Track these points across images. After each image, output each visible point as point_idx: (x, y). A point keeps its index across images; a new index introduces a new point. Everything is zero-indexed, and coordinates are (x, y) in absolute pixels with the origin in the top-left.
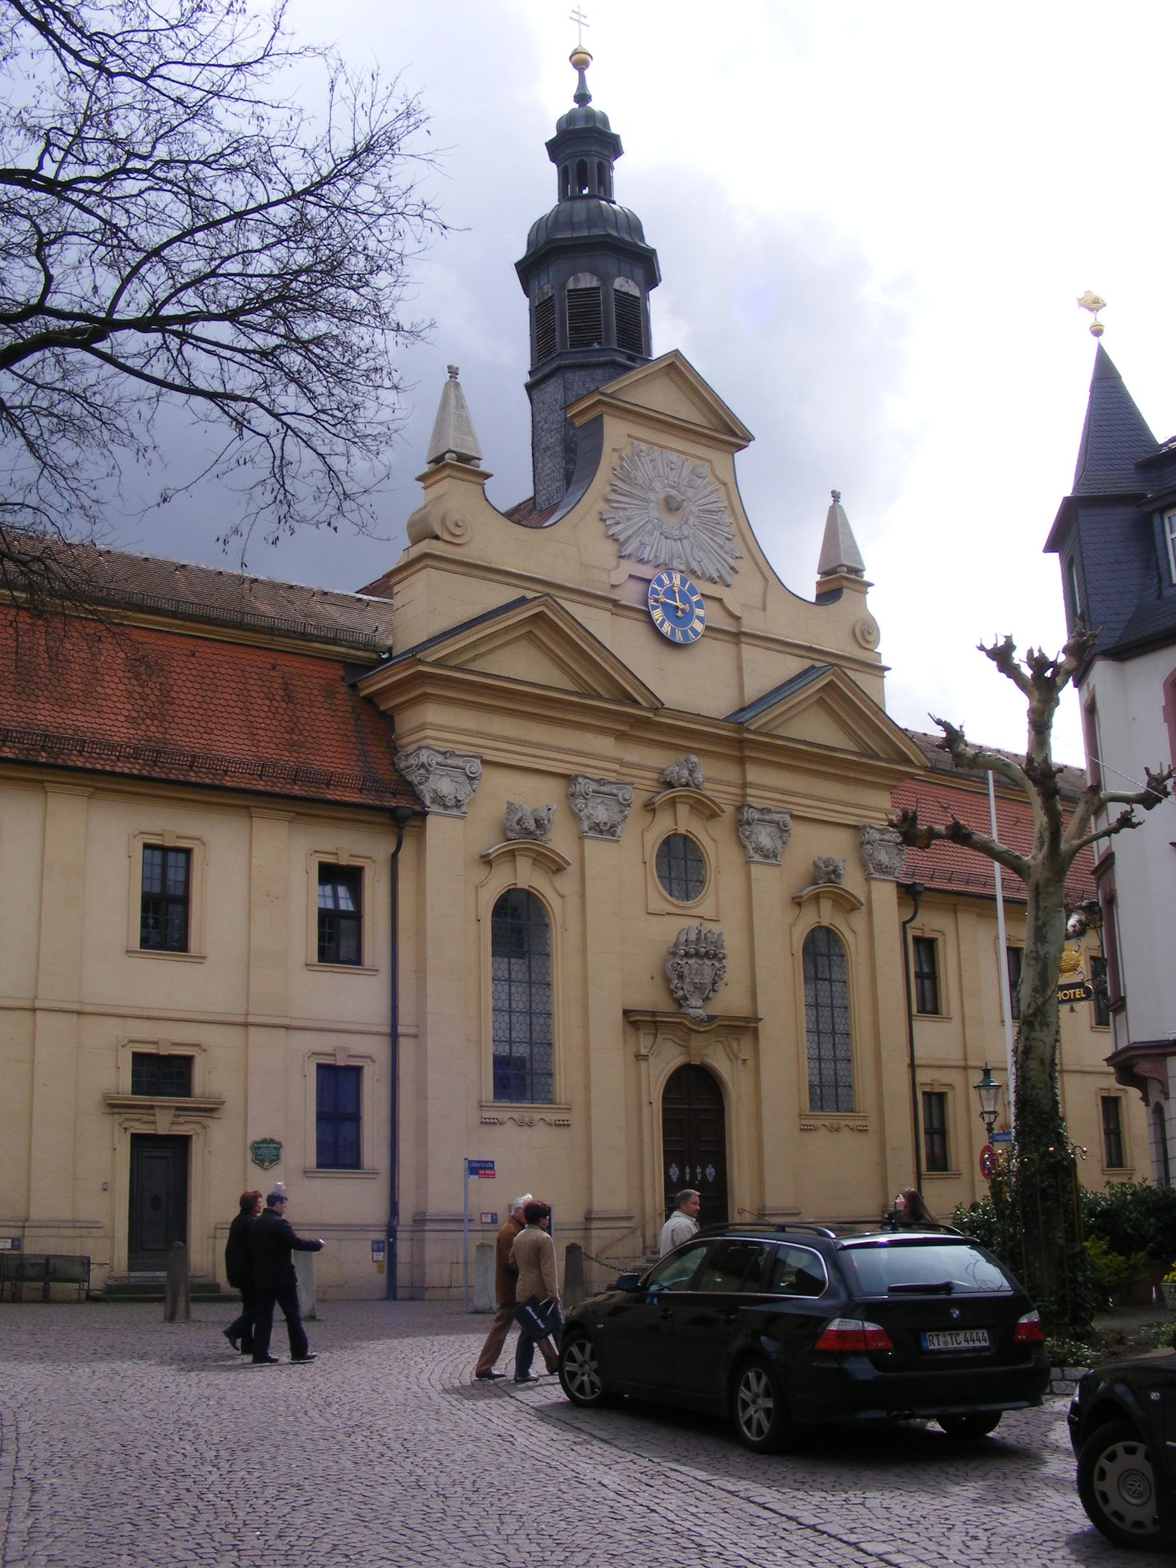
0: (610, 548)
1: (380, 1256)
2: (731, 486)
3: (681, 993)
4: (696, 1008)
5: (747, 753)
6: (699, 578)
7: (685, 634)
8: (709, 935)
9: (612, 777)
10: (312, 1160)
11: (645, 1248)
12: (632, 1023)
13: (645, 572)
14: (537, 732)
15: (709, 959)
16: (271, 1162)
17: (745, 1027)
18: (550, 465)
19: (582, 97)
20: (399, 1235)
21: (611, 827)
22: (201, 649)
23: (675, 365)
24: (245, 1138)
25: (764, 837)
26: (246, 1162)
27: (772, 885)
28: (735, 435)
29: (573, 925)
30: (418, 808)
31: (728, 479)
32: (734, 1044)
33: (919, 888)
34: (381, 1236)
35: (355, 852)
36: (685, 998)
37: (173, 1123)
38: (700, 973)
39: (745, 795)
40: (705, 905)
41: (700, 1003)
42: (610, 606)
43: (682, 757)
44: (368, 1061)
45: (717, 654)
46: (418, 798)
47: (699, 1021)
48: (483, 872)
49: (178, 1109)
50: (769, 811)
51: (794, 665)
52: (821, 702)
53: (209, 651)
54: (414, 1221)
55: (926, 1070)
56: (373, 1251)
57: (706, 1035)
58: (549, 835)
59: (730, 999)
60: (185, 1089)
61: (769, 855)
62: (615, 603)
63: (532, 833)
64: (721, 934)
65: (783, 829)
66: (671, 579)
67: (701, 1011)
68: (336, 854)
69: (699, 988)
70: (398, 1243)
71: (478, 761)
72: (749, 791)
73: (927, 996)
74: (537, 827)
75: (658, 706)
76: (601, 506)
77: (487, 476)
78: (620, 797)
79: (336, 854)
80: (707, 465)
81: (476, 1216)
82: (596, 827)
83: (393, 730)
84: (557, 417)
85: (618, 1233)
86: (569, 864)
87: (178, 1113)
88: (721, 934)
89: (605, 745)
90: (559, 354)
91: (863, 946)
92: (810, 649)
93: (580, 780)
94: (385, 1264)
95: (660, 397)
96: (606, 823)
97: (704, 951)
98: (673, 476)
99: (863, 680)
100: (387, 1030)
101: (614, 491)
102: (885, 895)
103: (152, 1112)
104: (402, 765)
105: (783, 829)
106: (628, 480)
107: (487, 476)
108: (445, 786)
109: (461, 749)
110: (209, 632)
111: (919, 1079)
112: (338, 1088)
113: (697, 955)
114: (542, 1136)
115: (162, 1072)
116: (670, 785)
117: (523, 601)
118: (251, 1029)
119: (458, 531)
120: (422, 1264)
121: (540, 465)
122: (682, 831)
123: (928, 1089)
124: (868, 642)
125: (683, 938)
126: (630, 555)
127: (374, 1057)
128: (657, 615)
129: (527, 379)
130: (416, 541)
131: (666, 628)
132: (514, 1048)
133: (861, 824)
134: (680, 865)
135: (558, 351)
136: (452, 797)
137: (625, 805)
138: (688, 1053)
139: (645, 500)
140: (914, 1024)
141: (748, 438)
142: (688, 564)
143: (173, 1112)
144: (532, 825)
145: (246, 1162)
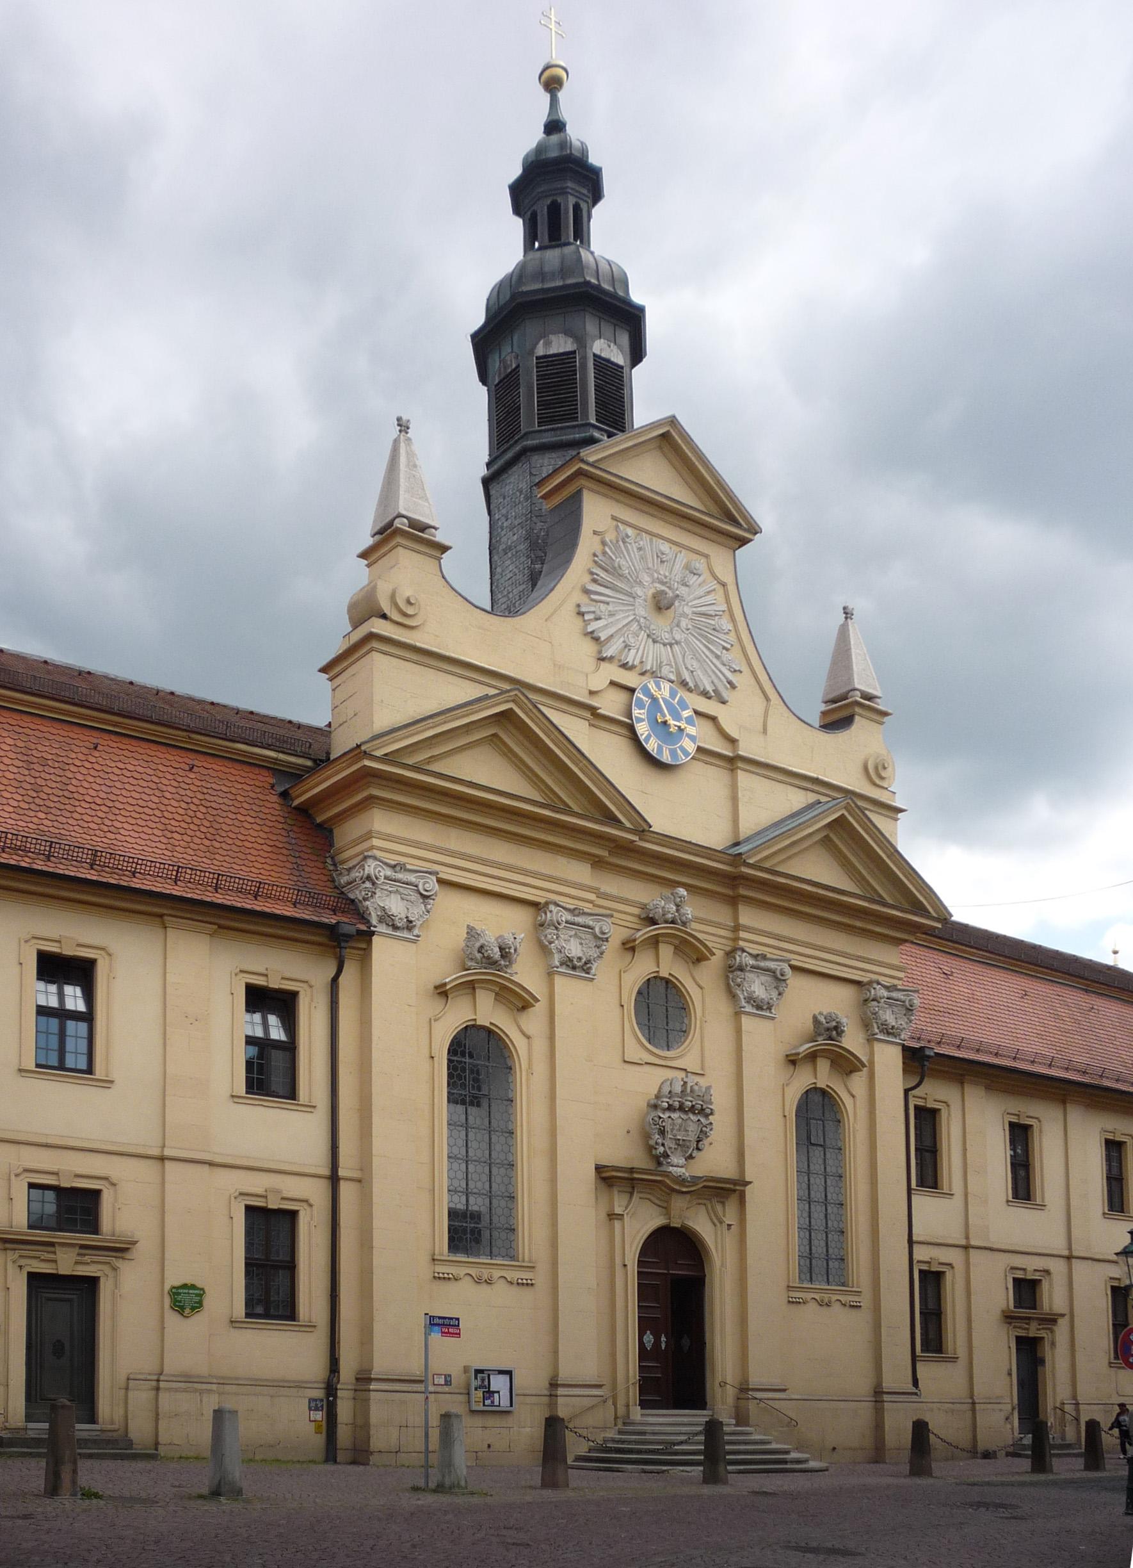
0: (588, 648)
1: (319, 1416)
2: (732, 588)
3: (661, 1149)
4: (678, 1166)
5: (742, 891)
6: (690, 690)
7: (673, 753)
8: (696, 1088)
9: (587, 907)
10: (240, 1309)
11: (616, 1418)
12: (604, 1179)
15: (694, 1113)
16: (193, 1309)
18: (511, 568)
19: (554, 126)
20: (339, 1393)
21: (586, 963)
23: (670, 441)
24: (163, 1282)
25: (758, 987)
26: (163, 1308)
27: (766, 1042)
28: (733, 521)
29: (540, 1068)
30: (363, 927)
31: (729, 579)
32: (719, 1208)
33: (928, 1052)
34: (319, 1394)
35: (288, 975)
37: (77, 1263)
40: (688, 1056)
41: (682, 1161)
42: (588, 715)
43: (667, 892)
44: (305, 1205)
45: (708, 782)
46: (363, 917)
47: (681, 1181)
48: (438, 1004)
49: (83, 1247)
50: (765, 957)
51: (796, 799)
52: (826, 842)
54: (357, 1379)
55: (924, 1247)
56: (310, 1409)
57: (688, 1197)
58: (515, 967)
59: (715, 1161)
60: (92, 1224)
61: (762, 1007)
62: (593, 710)
63: (493, 963)
64: (709, 1088)
65: (778, 979)
67: (683, 1170)
68: (266, 976)
69: (681, 1145)
70: (339, 1402)
71: (434, 879)
72: (742, 934)
73: (927, 1169)
74: (502, 956)
75: (643, 828)
76: (578, 597)
77: (444, 549)
78: (597, 930)
80: (703, 560)
83: (331, 845)
85: (587, 1402)
86: (537, 1000)
88: (709, 1088)
89: (580, 872)
90: (525, 434)
91: (862, 1112)
92: (816, 781)
93: (552, 907)
94: (324, 1423)
95: (652, 475)
96: (580, 959)
97: (695, 1107)
98: (663, 570)
100: (326, 1171)
101: (595, 581)
102: (888, 1061)
103: (52, 1249)
104: (344, 880)
105: (778, 979)
107: (444, 549)
108: (396, 906)
111: (916, 1257)
112: (270, 1233)
113: (681, 1108)
114: (501, 1295)
116: (652, 921)
117: (486, 697)
119: (410, 611)
120: (366, 1426)
121: (499, 570)
122: (664, 974)
123: (925, 1267)
125: (666, 1089)
127: (311, 1201)
128: (642, 729)
130: (356, 624)
131: (652, 746)
132: (472, 1200)
133: (865, 980)
134: (661, 1012)
136: (403, 916)
137: (601, 939)
139: (630, 595)
141: (755, 530)
142: (678, 674)
143: (77, 1250)
144: (496, 954)
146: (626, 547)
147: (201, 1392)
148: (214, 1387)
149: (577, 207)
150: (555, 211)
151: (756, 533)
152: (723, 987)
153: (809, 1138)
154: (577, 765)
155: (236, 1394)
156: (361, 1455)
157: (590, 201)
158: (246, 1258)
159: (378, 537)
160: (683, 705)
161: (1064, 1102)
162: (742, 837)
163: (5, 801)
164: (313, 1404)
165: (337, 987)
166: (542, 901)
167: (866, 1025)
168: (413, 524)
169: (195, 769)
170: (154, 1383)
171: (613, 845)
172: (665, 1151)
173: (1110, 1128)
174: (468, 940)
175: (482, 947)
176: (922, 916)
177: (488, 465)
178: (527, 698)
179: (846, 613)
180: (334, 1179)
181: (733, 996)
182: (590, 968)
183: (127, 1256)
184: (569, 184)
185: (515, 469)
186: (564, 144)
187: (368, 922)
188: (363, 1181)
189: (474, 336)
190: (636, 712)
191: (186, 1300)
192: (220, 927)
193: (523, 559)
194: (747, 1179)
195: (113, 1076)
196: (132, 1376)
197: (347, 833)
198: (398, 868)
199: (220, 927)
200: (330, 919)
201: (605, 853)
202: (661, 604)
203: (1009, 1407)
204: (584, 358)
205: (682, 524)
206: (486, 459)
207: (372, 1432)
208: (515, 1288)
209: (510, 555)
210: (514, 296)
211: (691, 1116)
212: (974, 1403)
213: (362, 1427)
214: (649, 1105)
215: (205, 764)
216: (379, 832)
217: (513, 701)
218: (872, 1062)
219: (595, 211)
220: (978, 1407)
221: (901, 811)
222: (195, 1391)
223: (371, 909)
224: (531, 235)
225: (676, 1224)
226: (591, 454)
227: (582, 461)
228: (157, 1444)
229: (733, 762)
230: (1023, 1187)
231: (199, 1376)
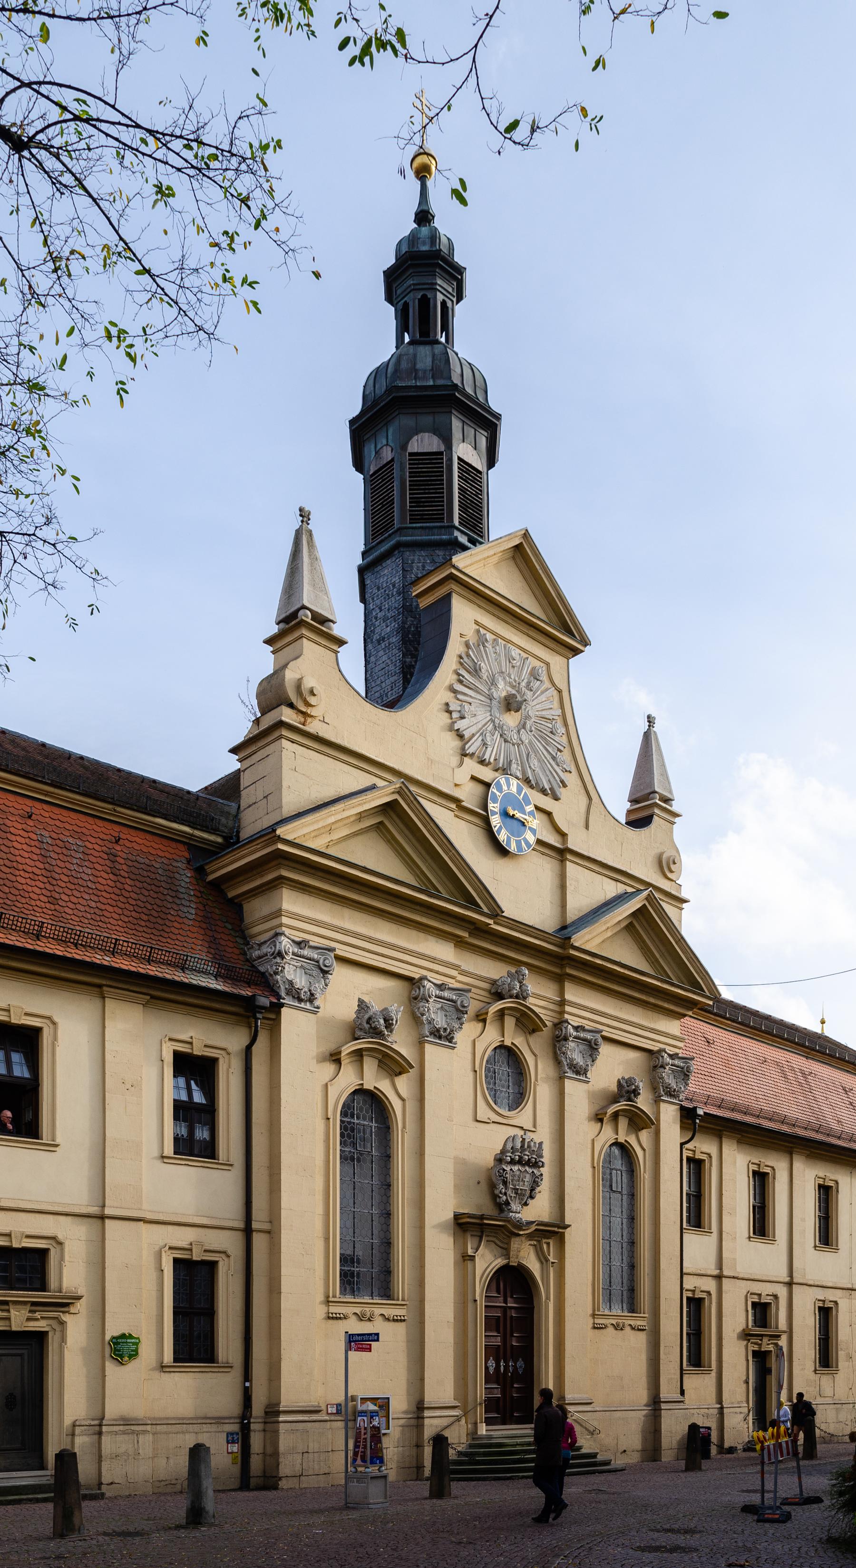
1: (235, 1448)
5: (569, 971)
6: (532, 787)
7: (518, 843)
13: (486, 774)
14: (385, 932)
15: (530, 1166)
17: (552, 1233)
18: (384, 658)
19: (423, 217)
20: (253, 1427)
21: (450, 1033)
22: (38, 812)
23: (523, 555)
26: (103, 1357)
31: (562, 686)
34: (235, 1428)
36: (507, 1203)
37: (28, 1319)
38: (521, 1180)
39: (562, 1012)
42: (453, 806)
44: (223, 1256)
45: (543, 869)
46: (271, 989)
49: (34, 1304)
51: (611, 889)
53: (47, 815)
54: (266, 1413)
56: (228, 1442)
59: (538, 1210)
61: (580, 1072)
62: (457, 801)
65: (592, 1049)
66: (508, 785)
73: (695, 1215)
75: (496, 913)
76: (448, 697)
77: (341, 642)
78: (459, 1003)
79: (191, 1043)
81: (323, 1407)
82: (436, 1033)
83: (242, 920)
84: (396, 601)
87: (34, 1308)
89: (445, 951)
90: (398, 529)
94: (239, 1455)
96: (445, 1029)
99: (669, 909)
100: (241, 1225)
101: (460, 682)
102: (669, 1115)
103: (6, 1307)
106: (476, 671)
108: (301, 981)
109: (315, 941)
110: (47, 794)
111: (685, 1286)
112: (194, 1280)
113: (520, 1162)
117: (373, 787)
118: (107, 1221)
120: (276, 1454)
121: (373, 659)
124: (671, 872)
125: (509, 1146)
126: (473, 754)
127: (229, 1253)
128: (496, 821)
129: (359, 561)
130: (265, 709)
131: (502, 837)
134: (508, 1077)
135: (397, 525)
140: (685, 1236)
141: (586, 642)
143: (28, 1307)
145: (103, 1357)
146: (485, 651)
147: (138, 1433)
148: (149, 1428)
149: (444, 303)
150: (425, 305)
151: (586, 646)
152: (551, 1055)
153: (611, 1186)
154: (447, 854)
155: (166, 1433)
156: (270, 1481)
157: (455, 300)
158: (174, 1307)
159: (282, 625)
160: (527, 801)
161: (791, 1154)
162: (569, 920)
163: (4, 876)
164: (230, 1438)
165: (251, 1054)
166: (417, 976)
167: (654, 1089)
168: (317, 617)
169: (121, 842)
170: (97, 1428)
171: (472, 927)
172: (507, 1200)
173: (821, 1174)
174: (358, 1012)
175: (370, 1019)
176: (699, 994)
177: (364, 554)
178: (410, 791)
179: (649, 722)
180: (248, 1231)
181: (558, 1062)
182: (453, 1038)
183: (72, 1310)
184: (439, 282)
185: (389, 562)
186: (434, 236)
187: (279, 997)
188: (273, 1233)
189: (352, 422)
190: (491, 806)
191: (122, 1349)
192: (153, 997)
193: (395, 651)
194: (567, 1223)
195: (58, 1141)
196: (77, 1423)
197: (256, 909)
198: (303, 945)
199: (153, 997)
200: (247, 992)
201: (466, 935)
202: (511, 704)
203: (746, 1410)
204: (450, 460)
205: (530, 633)
206: (362, 548)
207: (281, 1460)
208: (392, 1324)
209: (383, 645)
210: (389, 390)
211: (527, 1168)
213: (273, 1455)
214: (495, 1159)
215: (129, 837)
216: (287, 912)
217: (398, 793)
218: (658, 1120)
219: (457, 308)
220: (725, 1410)
221: (686, 901)
222: (133, 1432)
223: (280, 982)
224: (403, 326)
225: (514, 1264)
226: (460, 560)
227: (454, 567)
228: (100, 1484)
229: (562, 853)
230: (761, 1226)
231: (136, 1419)
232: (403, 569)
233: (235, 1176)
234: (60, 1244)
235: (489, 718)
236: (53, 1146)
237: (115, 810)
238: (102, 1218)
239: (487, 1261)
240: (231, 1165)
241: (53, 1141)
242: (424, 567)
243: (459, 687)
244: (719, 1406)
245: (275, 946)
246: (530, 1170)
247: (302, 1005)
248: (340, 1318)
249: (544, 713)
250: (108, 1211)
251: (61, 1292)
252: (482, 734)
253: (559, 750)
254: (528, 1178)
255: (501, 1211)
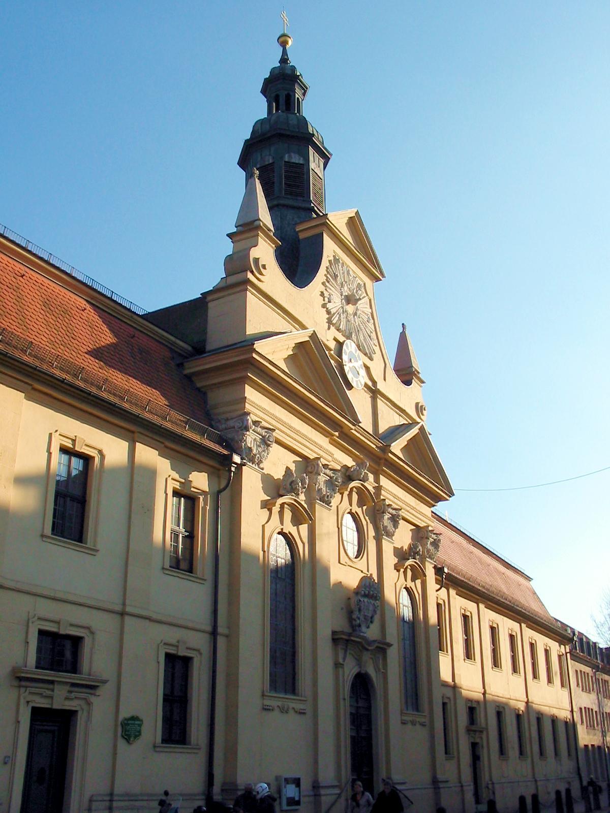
10: (159, 739)
13: (341, 339)
19: (284, 60)
36: (359, 626)
37: (67, 699)
49: (73, 685)
60: (74, 667)
76: (323, 288)
100: (209, 628)
115: (60, 651)
127: (202, 651)
138: (360, 667)
143: (68, 688)
175: (292, 482)
180: (214, 633)
191: (129, 729)
195: (99, 547)
196: (95, 798)
198: (257, 424)
212: (536, 781)
225: (363, 672)
232: (281, 218)
233: (207, 587)
234: (92, 633)
235: (341, 305)
236: (94, 551)
237: (132, 317)
238: (122, 614)
239: (350, 670)
240: (205, 580)
241: (94, 546)
242: (293, 218)
243: (327, 284)
244: (460, 785)
245: (243, 422)
246: (373, 602)
247: (254, 466)
248: (269, 710)
249: (364, 309)
250: (128, 609)
251: (26, 667)
252: (338, 313)
253: (371, 332)
254: (371, 608)
255: (354, 630)
